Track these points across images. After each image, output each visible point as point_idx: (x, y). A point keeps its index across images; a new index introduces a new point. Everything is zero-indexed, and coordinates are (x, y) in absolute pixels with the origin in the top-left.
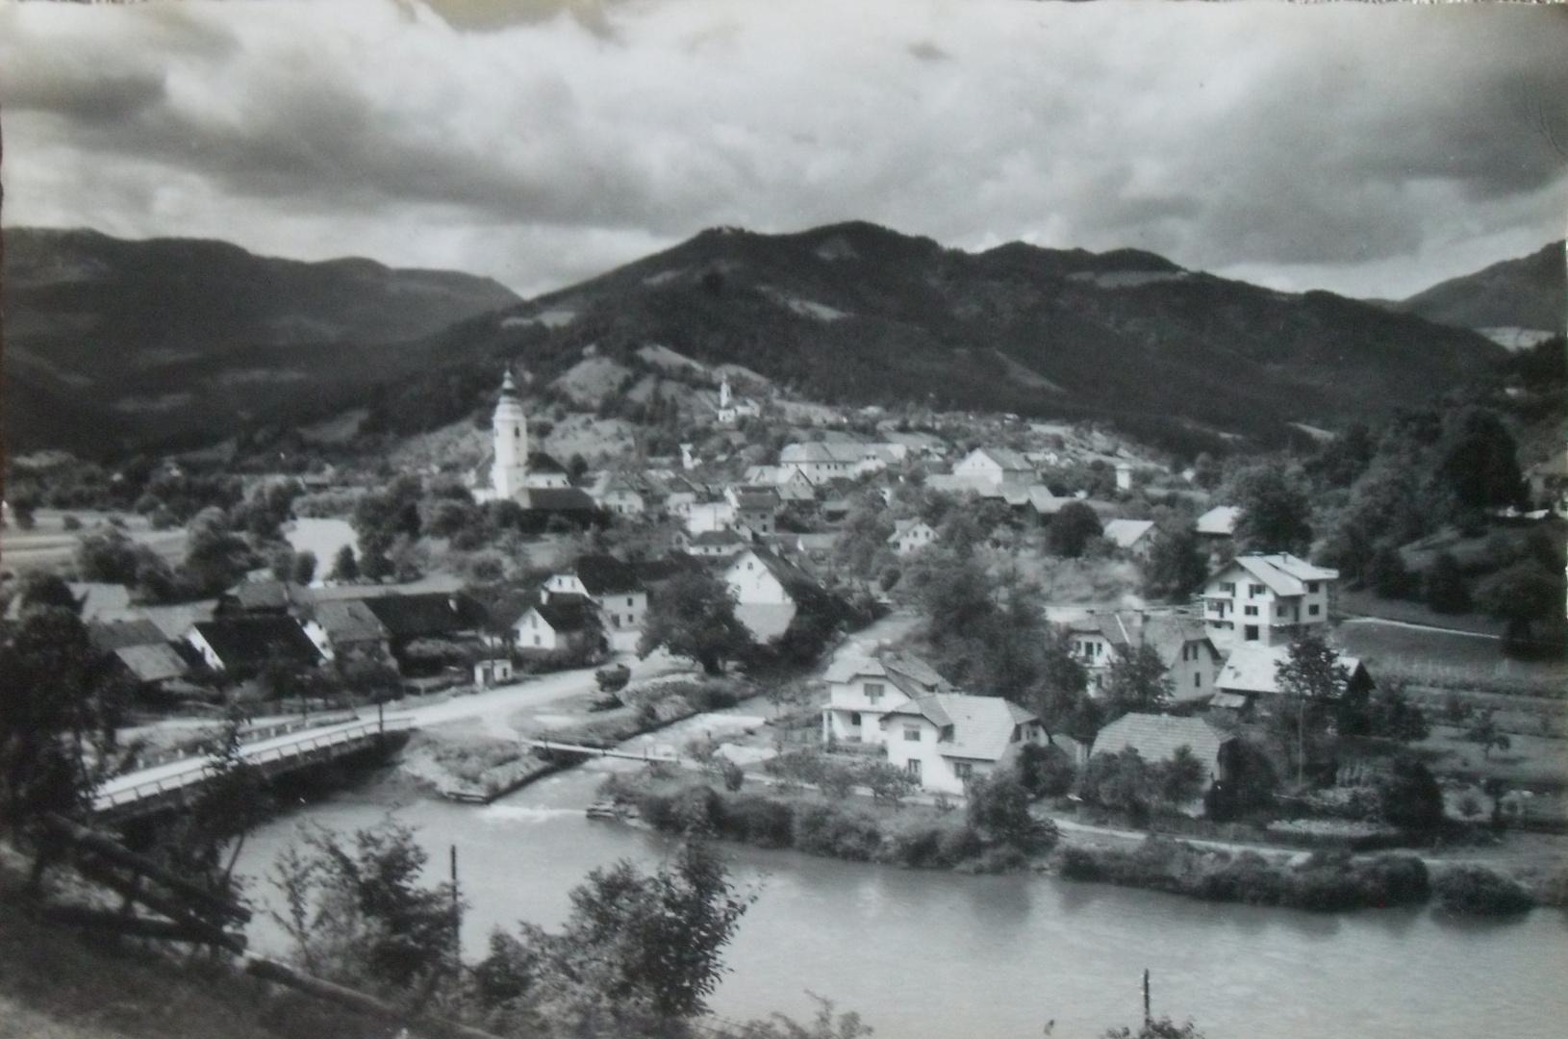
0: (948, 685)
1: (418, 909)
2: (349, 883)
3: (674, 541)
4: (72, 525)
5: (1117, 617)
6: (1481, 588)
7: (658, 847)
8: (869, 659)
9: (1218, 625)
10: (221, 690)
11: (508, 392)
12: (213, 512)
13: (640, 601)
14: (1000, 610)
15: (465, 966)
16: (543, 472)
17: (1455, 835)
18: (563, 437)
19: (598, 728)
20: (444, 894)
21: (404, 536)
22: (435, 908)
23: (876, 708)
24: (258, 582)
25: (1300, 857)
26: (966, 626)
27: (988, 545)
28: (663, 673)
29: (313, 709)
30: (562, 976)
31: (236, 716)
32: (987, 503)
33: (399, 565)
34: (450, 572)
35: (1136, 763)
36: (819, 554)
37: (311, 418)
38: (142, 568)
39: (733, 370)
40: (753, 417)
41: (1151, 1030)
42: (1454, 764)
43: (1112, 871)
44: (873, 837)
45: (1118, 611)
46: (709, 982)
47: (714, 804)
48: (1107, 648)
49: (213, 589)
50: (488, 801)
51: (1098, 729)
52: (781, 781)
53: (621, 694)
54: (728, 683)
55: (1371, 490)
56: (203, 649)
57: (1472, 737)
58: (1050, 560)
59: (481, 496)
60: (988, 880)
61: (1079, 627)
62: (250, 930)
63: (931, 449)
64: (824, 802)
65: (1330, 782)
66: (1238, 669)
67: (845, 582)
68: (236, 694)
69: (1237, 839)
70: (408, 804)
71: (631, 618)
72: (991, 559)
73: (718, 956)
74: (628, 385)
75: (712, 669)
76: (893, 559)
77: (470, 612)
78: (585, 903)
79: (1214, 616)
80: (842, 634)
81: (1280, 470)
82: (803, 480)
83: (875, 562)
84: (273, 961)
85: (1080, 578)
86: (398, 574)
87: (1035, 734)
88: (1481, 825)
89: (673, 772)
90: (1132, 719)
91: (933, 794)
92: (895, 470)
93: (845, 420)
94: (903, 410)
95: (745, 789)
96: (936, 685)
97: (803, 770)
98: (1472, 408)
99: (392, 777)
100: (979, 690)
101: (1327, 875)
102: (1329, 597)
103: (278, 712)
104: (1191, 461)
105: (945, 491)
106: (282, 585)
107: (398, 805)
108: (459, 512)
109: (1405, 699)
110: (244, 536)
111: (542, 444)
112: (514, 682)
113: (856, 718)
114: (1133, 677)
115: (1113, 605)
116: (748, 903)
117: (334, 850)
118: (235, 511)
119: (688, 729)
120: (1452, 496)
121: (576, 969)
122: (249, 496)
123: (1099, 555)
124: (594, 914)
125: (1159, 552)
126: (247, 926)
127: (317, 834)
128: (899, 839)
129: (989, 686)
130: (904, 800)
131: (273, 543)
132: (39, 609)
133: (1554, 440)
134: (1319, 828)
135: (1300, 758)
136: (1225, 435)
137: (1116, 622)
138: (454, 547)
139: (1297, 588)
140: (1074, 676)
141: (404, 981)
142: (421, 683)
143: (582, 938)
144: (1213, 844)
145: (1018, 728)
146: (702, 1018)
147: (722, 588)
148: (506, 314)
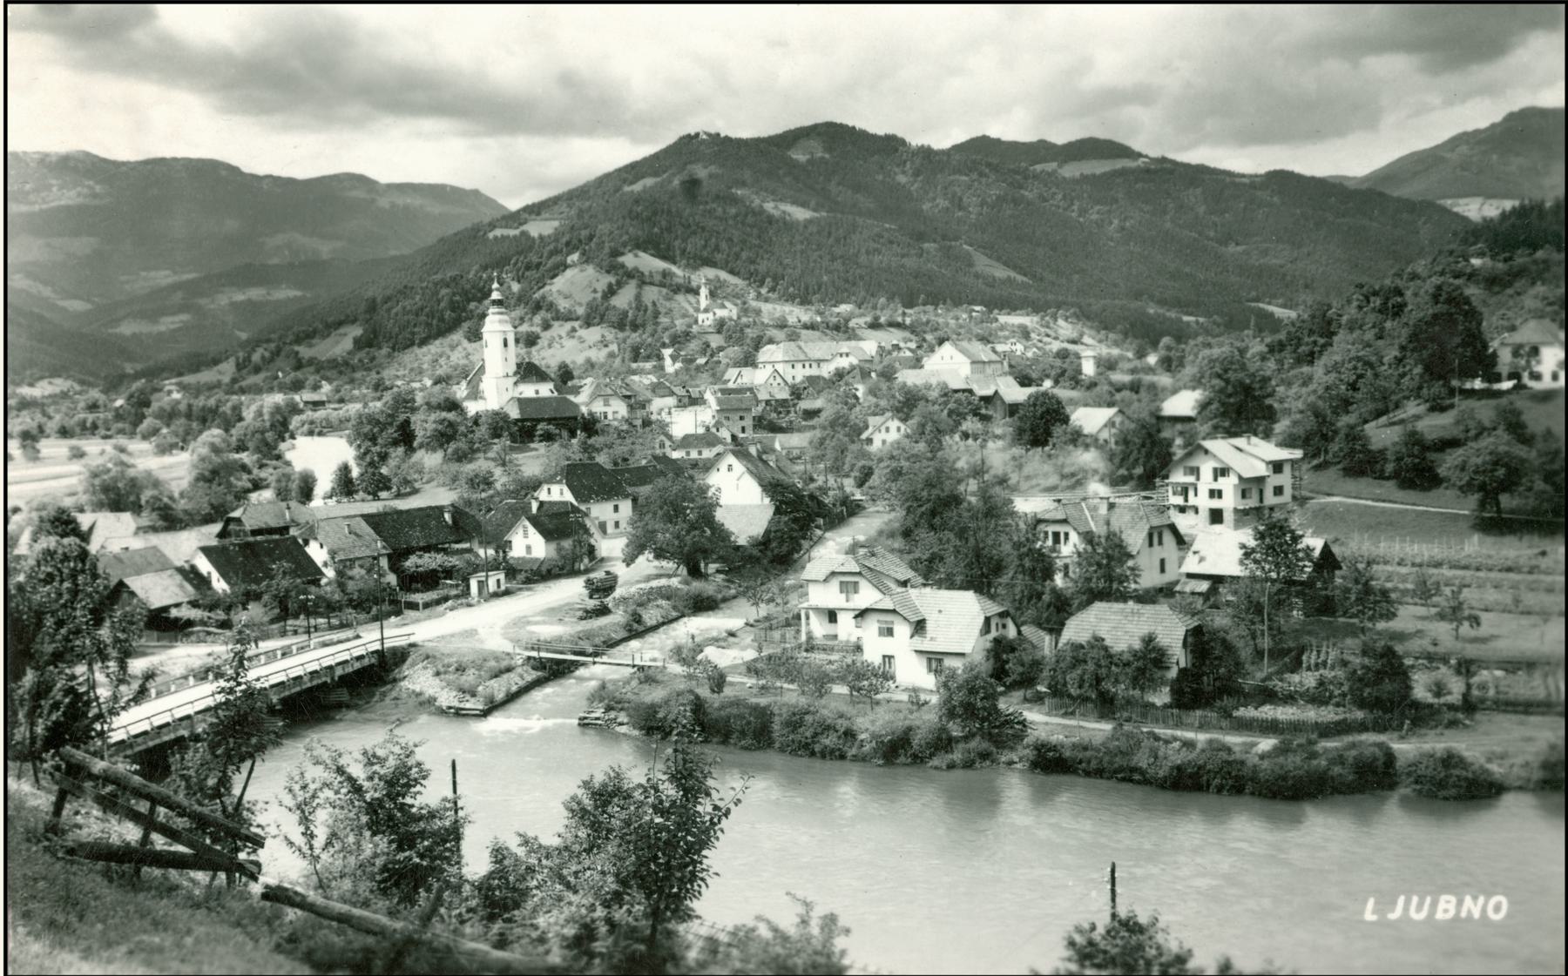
0: (920, 580)
1: (422, 824)
2: (357, 803)
3: (657, 446)
4: (78, 454)
5: (1083, 504)
6: (1447, 463)
7: (649, 754)
8: (844, 556)
9: (1182, 510)
10: (228, 614)
11: (495, 303)
12: (214, 434)
13: (626, 507)
14: (969, 503)
15: (467, 881)
16: (531, 382)
17: (1421, 717)
18: (550, 346)
19: (588, 636)
20: (447, 809)
21: (401, 450)
22: (438, 823)
23: (851, 605)
24: (260, 503)
25: (1266, 744)
26: (937, 521)
27: (957, 437)
28: (649, 578)
29: (316, 629)
30: (559, 887)
31: (242, 640)
32: (959, 395)
33: (395, 480)
34: (444, 485)
35: (1103, 653)
36: (795, 453)
37: (307, 337)
38: (146, 496)
39: (711, 272)
40: (731, 319)
41: (1116, 924)
42: (1415, 645)
43: (1080, 762)
44: (850, 734)
45: (1084, 499)
46: (696, 888)
47: (698, 706)
48: (1074, 537)
49: (217, 513)
50: (485, 714)
51: (1067, 619)
52: (763, 682)
53: (609, 601)
54: (711, 586)
55: (1336, 368)
56: (209, 573)
57: (1442, 616)
58: (1017, 451)
59: (472, 408)
60: (958, 774)
61: (1047, 517)
62: (263, 855)
63: (902, 345)
64: (803, 701)
65: (1296, 666)
66: (1202, 554)
67: (820, 481)
68: (241, 617)
69: (1202, 727)
70: (410, 721)
71: (617, 524)
72: (960, 452)
73: (705, 861)
74: (611, 291)
75: (695, 572)
76: (865, 455)
77: (463, 525)
78: (579, 812)
79: (1179, 500)
80: (819, 532)
81: (1242, 352)
82: (779, 380)
83: (849, 459)
84: (286, 885)
85: (1047, 468)
86: (394, 489)
87: (1004, 626)
88: (1451, 707)
89: (659, 677)
90: (1099, 607)
91: (906, 690)
92: (867, 365)
93: (819, 319)
94: (875, 307)
95: (728, 692)
96: (909, 580)
97: (782, 670)
98: (1436, 280)
99: (394, 694)
100: (949, 584)
101: (1294, 761)
102: (1294, 477)
103: (283, 634)
104: (1155, 345)
105: (916, 386)
106: (284, 504)
107: (400, 722)
108: (451, 424)
109: (1372, 578)
110: (245, 457)
111: (529, 353)
112: (507, 593)
113: (832, 616)
114: (1099, 565)
115: (1079, 493)
116: (732, 806)
117: (340, 770)
118: (236, 432)
119: (673, 634)
120: (1418, 370)
121: (572, 879)
122: (249, 414)
123: (1065, 443)
124: (587, 823)
125: (1124, 440)
126: (260, 851)
127: (325, 756)
128: (874, 736)
129: (959, 579)
130: (879, 697)
131: (274, 462)
132: (50, 542)
133: (1522, 308)
134: (1284, 713)
135: (1266, 643)
136: (1186, 318)
137: (1082, 510)
138: (447, 460)
139: (1261, 470)
140: (1042, 567)
141: (410, 899)
142: (419, 598)
143: (576, 848)
144: (1179, 733)
145: (987, 620)
146: (690, 924)
147: (703, 490)
148: (492, 226)
